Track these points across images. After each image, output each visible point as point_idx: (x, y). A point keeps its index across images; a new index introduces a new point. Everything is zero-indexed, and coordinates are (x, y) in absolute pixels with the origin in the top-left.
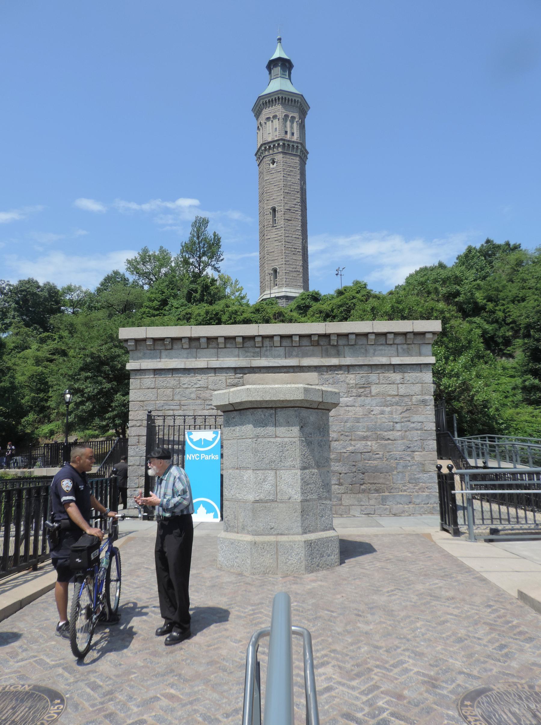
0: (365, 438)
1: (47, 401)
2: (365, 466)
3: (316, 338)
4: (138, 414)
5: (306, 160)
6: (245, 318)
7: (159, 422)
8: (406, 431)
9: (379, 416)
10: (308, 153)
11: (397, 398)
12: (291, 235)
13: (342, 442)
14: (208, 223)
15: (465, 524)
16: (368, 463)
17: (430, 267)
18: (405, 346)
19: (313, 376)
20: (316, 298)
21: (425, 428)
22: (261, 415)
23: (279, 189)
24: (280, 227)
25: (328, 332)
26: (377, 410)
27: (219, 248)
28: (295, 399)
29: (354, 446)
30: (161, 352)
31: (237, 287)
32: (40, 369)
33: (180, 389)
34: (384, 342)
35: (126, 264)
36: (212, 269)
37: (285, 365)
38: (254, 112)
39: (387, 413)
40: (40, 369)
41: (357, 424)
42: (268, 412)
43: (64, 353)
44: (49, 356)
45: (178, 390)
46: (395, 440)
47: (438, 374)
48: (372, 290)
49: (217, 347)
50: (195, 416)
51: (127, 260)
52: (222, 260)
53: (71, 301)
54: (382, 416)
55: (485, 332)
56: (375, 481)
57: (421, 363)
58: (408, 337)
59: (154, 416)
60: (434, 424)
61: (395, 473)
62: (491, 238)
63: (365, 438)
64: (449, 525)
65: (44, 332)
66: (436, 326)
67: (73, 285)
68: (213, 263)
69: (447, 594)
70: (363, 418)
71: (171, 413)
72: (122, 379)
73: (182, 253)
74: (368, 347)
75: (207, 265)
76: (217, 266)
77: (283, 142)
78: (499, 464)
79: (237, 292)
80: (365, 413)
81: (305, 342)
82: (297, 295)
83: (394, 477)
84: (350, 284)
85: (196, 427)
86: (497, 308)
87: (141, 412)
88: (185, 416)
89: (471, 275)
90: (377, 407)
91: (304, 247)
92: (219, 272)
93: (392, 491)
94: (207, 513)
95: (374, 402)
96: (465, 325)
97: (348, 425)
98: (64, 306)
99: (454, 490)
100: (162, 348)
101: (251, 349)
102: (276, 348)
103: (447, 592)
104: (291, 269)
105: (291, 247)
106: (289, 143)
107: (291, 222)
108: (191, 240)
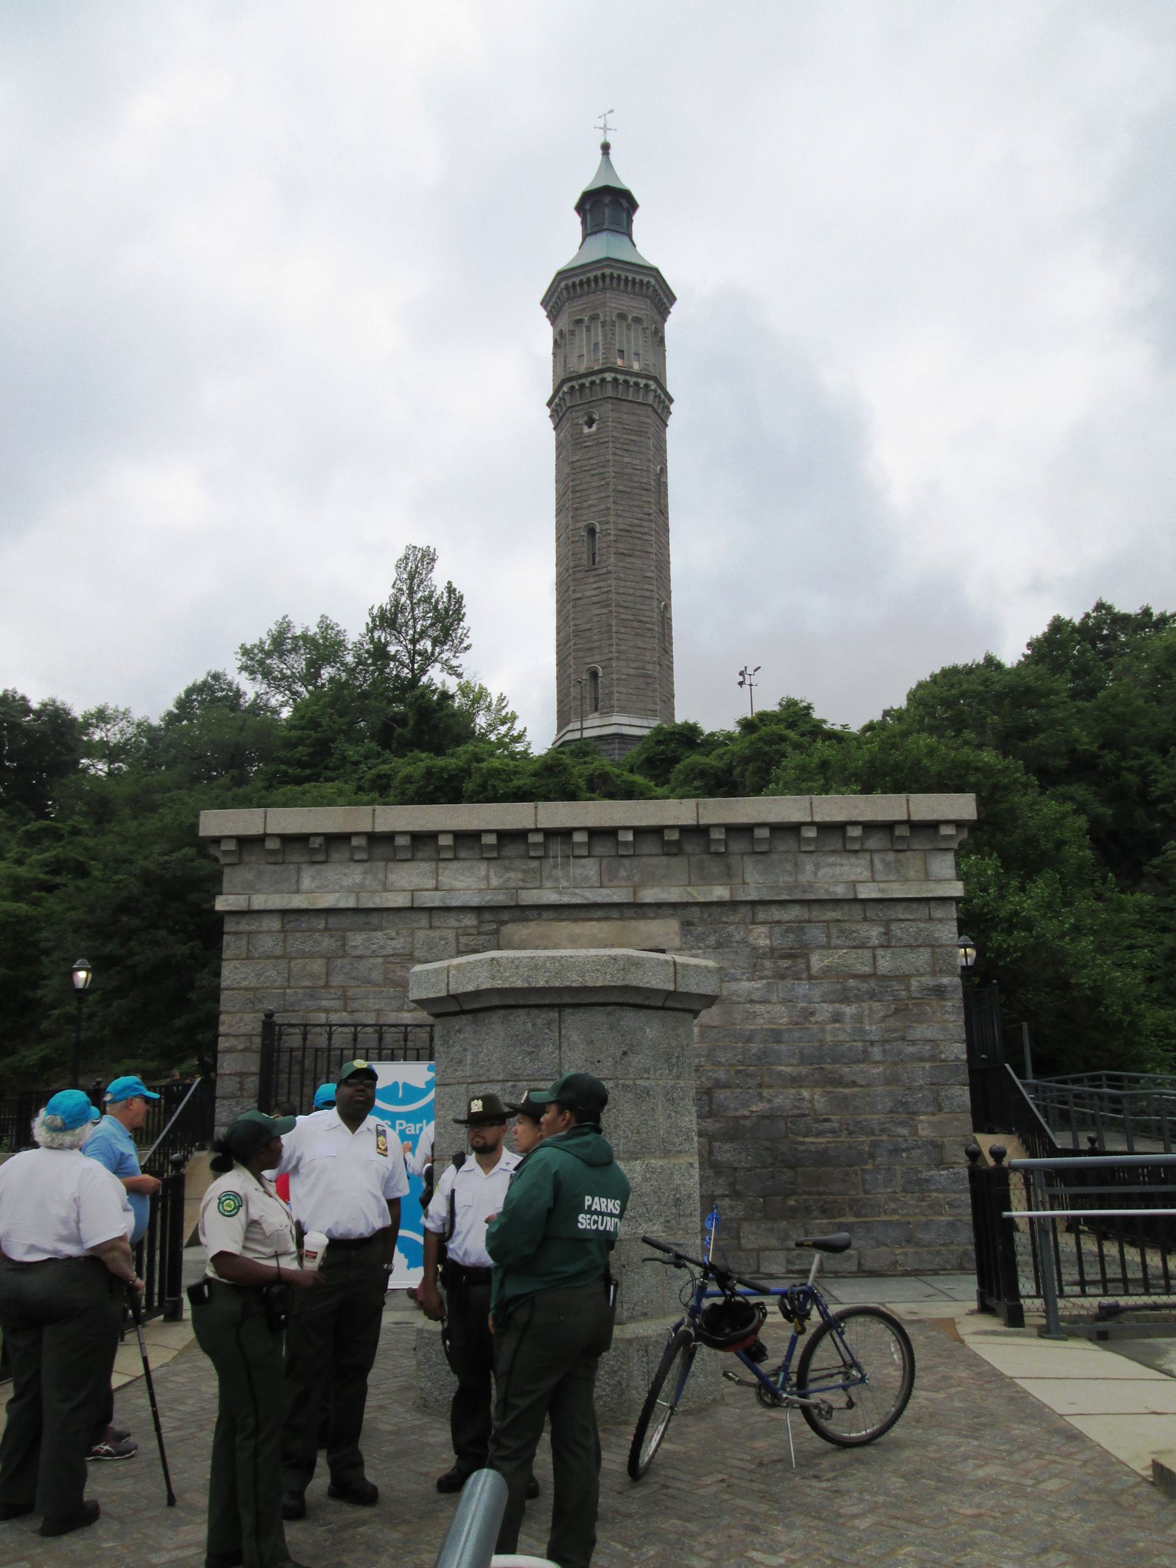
0: (796, 1081)
1: (35, 986)
2: (796, 1149)
3: (675, 836)
4: (241, 1020)
5: (667, 417)
6: (519, 788)
7: (293, 1040)
8: (895, 1064)
9: (829, 1027)
10: (671, 400)
11: (873, 984)
12: (631, 591)
13: (739, 1090)
14: (433, 560)
15: (1038, 1296)
16: (803, 1143)
17: (965, 666)
18: (891, 857)
19: (666, 929)
20: (689, 736)
21: (943, 1056)
22: (524, 1023)
23: (603, 482)
24: (604, 571)
25: (703, 821)
26: (825, 1011)
27: (461, 620)
28: (606, 983)
29: (770, 1101)
30: (299, 871)
31: (504, 713)
32: (23, 908)
33: (345, 961)
34: (839, 846)
35: (239, 657)
36: (442, 671)
37: (599, 900)
38: (545, 308)
39: (848, 1019)
40: (23, 908)
41: (776, 1047)
42: (542, 1017)
43: (81, 871)
44: (41, 876)
45: (339, 962)
46: (869, 1085)
47: (973, 923)
48: (825, 721)
49: (435, 856)
50: (381, 1026)
51: (243, 647)
52: (466, 648)
53: (103, 743)
54: (837, 1025)
55: (1096, 823)
56: (822, 1189)
57: (930, 895)
58: (897, 833)
59: (280, 1025)
60: (964, 1046)
61: (869, 1167)
62: (1108, 601)
63: (796, 1081)
64: (999, 1299)
65: (36, 820)
66: (963, 806)
67: (112, 706)
68: (445, 656)
69: (981, 1473)
70: (789, 1031)
71: (322, 1018)
72: (209, 931)
73: (371, 631)
74: (802, 857)
75: (429, 659)
76: (454, 663)
77: (613, 375)
78: (1130, 1145)
79: (503, 724)
80: (795, 1019)
81: (649, 846)
82: (646, 732)
83: (867, 1177)
84: (771, 705)
85: (384, 1052)
86: (1123, 764)
87: (248, 1017)
88: (356, 1026)
89: (1064, 684)
90: (825, 1005)
91: (663, 617)
92: (460, 676)
93: (863, 1211)
94: (409, 1267)
95: (817, 993)
96: (1051, 808)
97: (755, 1048)
98: (88, 756)
99: (1010, 1210)
100: (303, 859)
101: (518, 863)
102: (577, 860)
103: (979, 1467)
104: (632, 671)
105: (632, 618)
106: (628, 378)
107: (631, 560)
108: (396, 604)
